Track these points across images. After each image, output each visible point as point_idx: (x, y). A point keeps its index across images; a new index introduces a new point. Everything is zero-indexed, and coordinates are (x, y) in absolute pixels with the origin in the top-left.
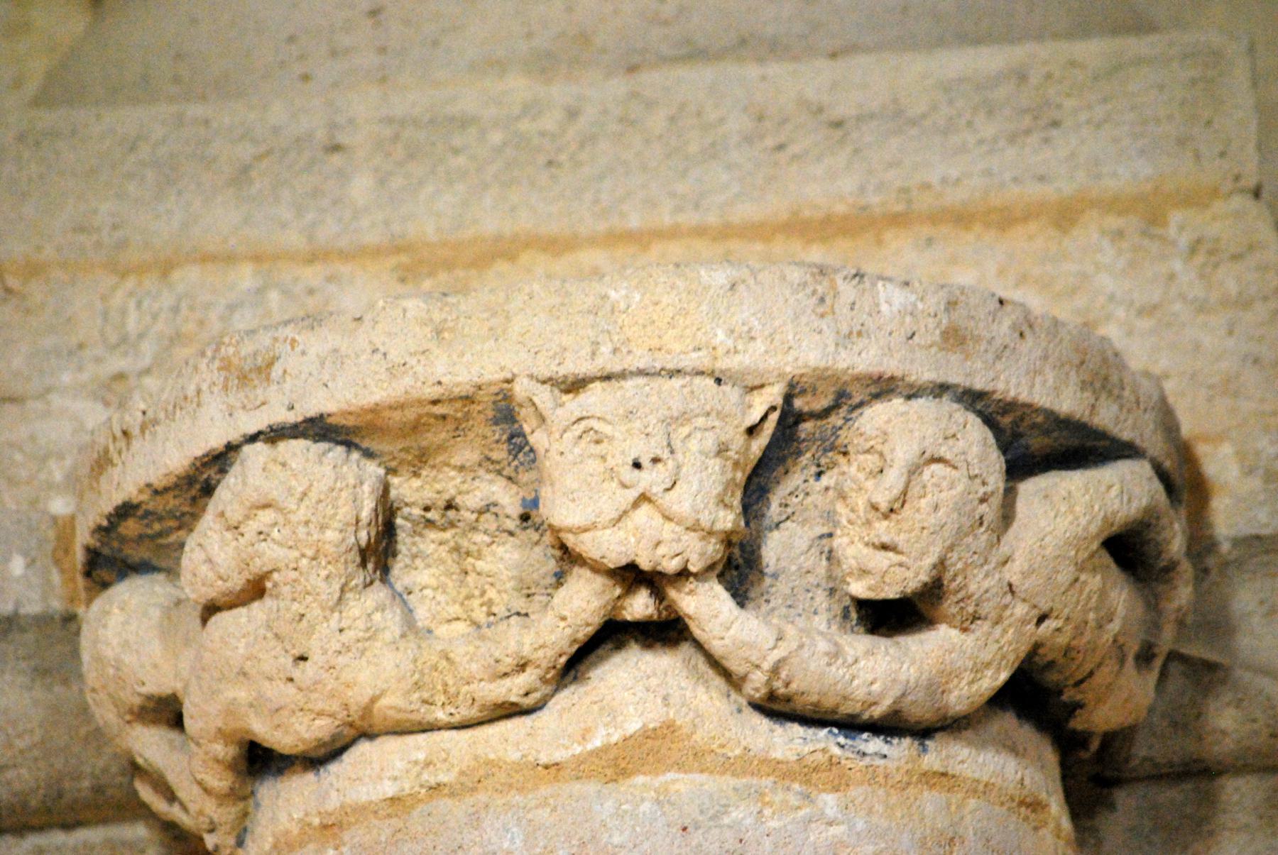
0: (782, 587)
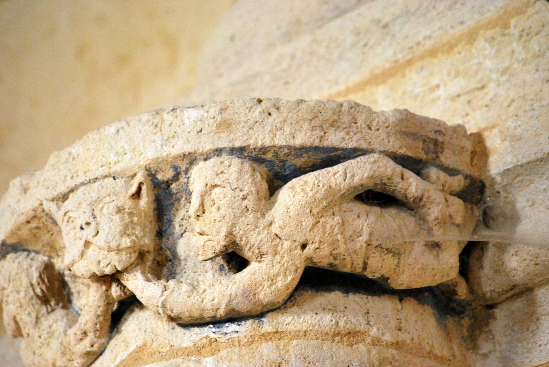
0: (190, 264)
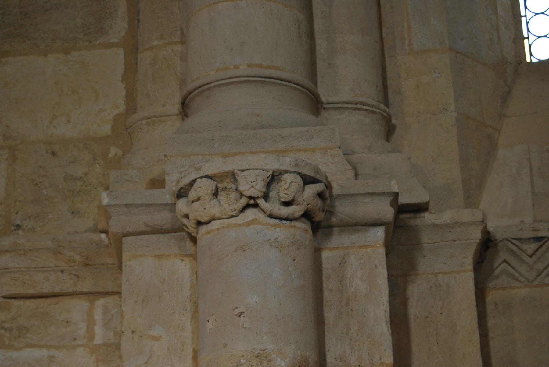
0: (272, 200)
